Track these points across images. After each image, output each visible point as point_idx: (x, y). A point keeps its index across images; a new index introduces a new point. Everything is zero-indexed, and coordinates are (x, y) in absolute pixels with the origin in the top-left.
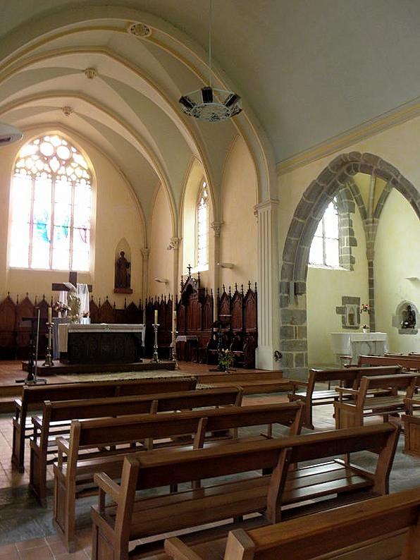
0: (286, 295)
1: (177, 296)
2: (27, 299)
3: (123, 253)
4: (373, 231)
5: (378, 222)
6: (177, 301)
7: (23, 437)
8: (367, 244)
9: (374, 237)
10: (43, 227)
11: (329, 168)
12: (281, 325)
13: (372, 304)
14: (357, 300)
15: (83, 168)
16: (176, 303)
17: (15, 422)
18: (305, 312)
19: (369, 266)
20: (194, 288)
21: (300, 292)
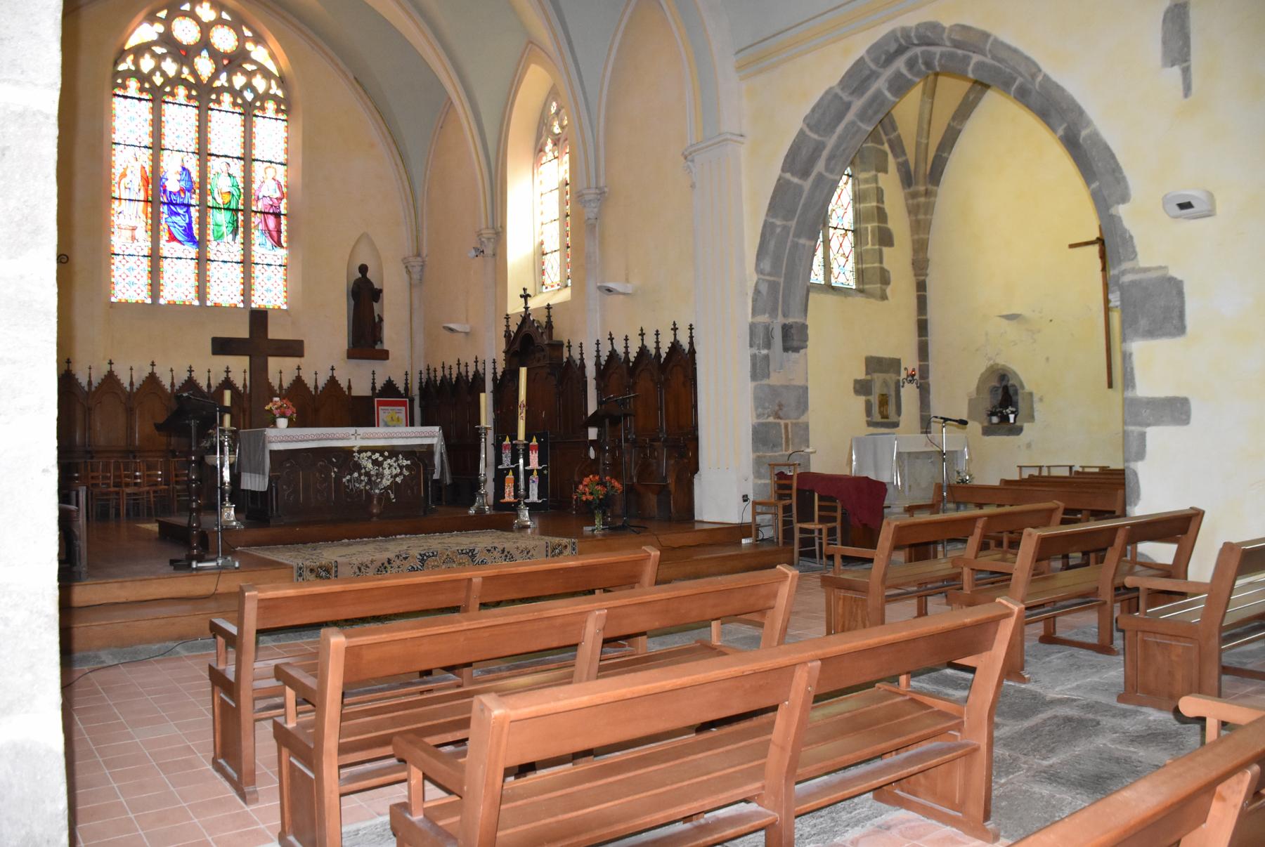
3: (363, 269)
4: (926, 213)
6: (495, 373)
8: (913, 242)
11: (867, 59)
12: (755, 421)
13: (924, 372)
14: (894, 365)
15: (267, 74)
19: (918, 290)
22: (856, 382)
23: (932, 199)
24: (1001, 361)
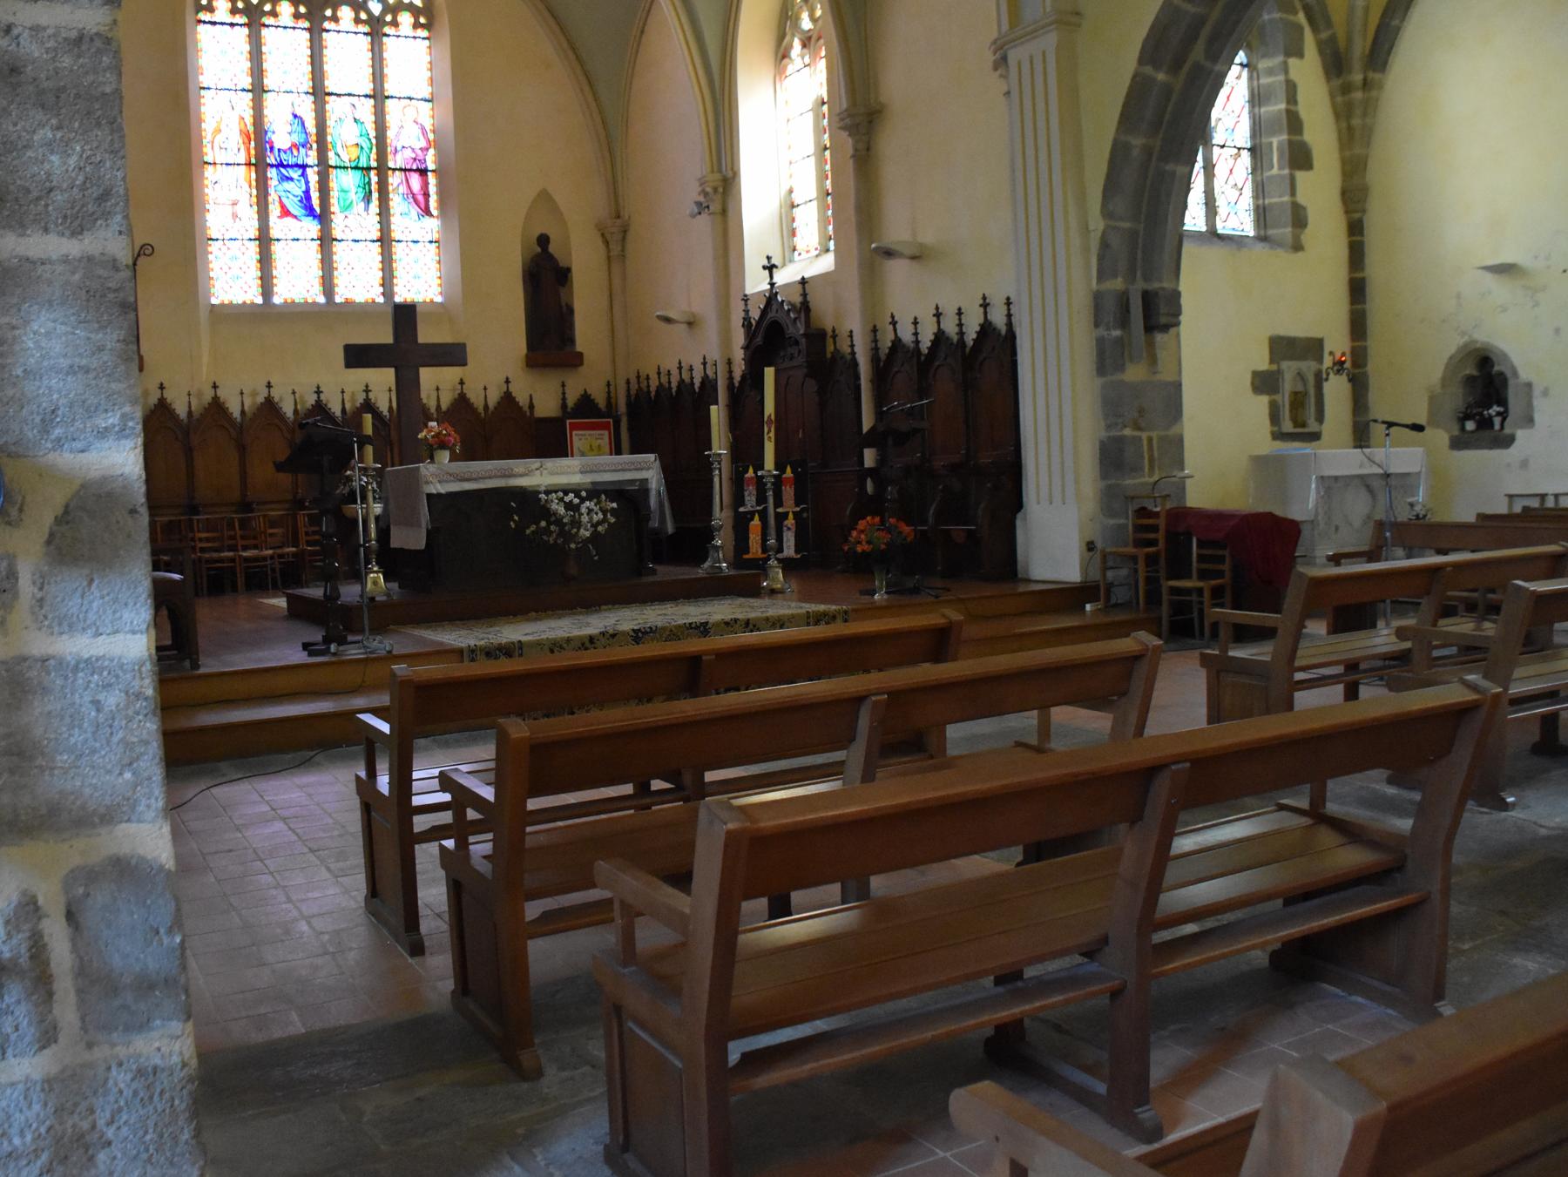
0: (1117, 333)
1: (729, 362)
2: (269, 401)
3: (543, 240)
4: (1365, 114)
5: (1381, 87)
6: (731, 378)
7: (408, 841)
9: (1367, 134)
10: (295, 173)
13: (1359, 356)
14: (1312, 348)
16: (730, 386)
17: (366, 788)
18: (1178, 386)
20: (791, 331)
21: (1163, 320)
22: (1256, 374)
23: (1374, 93)
24: (1482, 337)
